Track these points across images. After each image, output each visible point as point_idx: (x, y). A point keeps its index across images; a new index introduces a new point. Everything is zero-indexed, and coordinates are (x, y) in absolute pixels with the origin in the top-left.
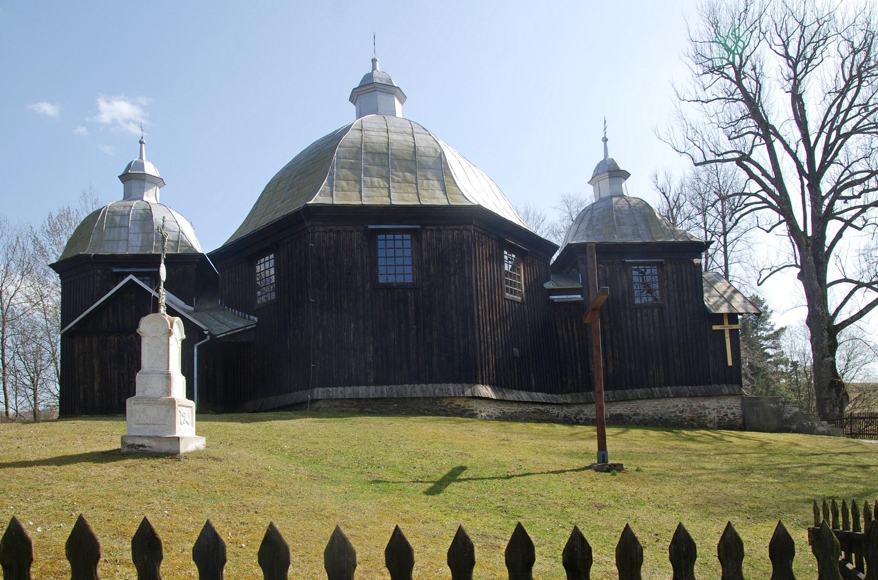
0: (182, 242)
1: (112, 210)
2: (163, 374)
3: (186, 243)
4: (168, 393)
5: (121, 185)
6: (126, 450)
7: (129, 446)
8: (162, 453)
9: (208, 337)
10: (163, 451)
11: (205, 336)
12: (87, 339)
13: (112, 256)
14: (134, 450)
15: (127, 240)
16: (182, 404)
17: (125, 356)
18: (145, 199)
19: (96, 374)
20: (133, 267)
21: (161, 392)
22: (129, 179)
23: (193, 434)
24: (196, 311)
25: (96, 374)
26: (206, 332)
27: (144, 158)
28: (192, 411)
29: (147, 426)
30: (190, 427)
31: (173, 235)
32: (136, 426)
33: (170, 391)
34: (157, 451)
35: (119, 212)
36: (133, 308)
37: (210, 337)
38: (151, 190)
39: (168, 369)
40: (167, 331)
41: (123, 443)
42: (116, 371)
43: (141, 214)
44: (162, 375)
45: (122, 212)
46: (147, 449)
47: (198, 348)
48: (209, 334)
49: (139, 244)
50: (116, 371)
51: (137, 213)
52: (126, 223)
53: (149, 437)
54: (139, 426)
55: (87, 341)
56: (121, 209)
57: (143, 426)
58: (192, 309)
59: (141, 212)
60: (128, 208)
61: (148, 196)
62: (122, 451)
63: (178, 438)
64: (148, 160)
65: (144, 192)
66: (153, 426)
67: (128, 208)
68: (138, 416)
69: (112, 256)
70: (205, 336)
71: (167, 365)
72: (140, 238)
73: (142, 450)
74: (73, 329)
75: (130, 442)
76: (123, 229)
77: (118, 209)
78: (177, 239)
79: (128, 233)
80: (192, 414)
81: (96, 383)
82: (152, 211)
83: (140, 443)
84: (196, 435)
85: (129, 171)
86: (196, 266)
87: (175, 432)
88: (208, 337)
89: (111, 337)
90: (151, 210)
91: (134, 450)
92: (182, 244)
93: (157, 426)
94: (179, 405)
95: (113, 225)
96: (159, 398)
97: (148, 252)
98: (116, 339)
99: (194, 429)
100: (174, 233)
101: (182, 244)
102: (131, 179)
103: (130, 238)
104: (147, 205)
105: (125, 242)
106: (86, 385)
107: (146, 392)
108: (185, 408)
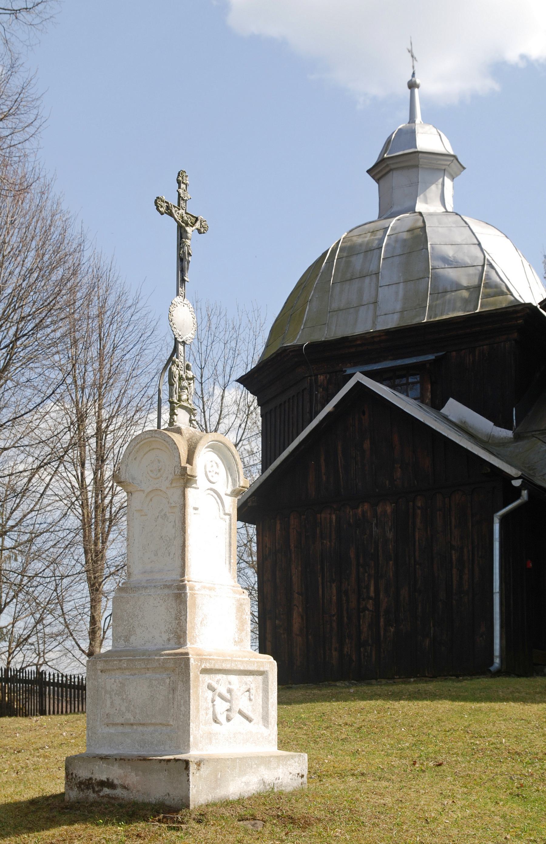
0: (487, 286)
1: (348, 244)
2: (169, 587)
3: (497, 286)
4: (179, 637)
5: (374, 185)
6: (74, 794)
7: (81, 783)
8: (149, 804)
9: (525, 493)
10: (153, 800)
11: (516, 493)
12: (278, 522)
13: (345, 339)
14: (92, 796)
15: (375, 303)
16: (217, 667)
17: (352, 555)
18: (420, 207)
19: (296, 595)
20: (385, 359)
21: (165, 637)
22: (388, 172)
23: (272, 748)
24: (518, 437)
25: (296, 595)
26: (517, 483)
27: (419, 119)
28: (266, 683)
29: (127, 729)
30: (257, 727)
31: (469, 275)
32: (107, 730)
33: (185, 633)
34: (140, 798)
35: (361, 245)
36: (367, 445)
37: (529, 495)
38: (433, 187)
39: (183, 574)
40: (178, 471)
41: (69, 777)
42: (334, 585)
43: (405, 240)
44: (166, 591)
45: (368, 243)
46: (119, 792)
47: (504, 520)
48: (527, 483)
49: (398, 307)
50: (334, 585)
51: (396, 241)
52: (373, 268)
53: (122, 760)
54: (112, 730)
55: (278, 527)
56: (367, 239)
57: (120, 729)
58: (508, 434)
59: (405, 236)
60: (379, 235)
61: (426, 201)
62: (66, 797)
63: (187, 763)
64: (426, 120)
65: (417, 197)
66: (140, 728)
67: (379, 235)
68: (108, 703)
69: (344, 341)
70: (516, 493)
71: (178, 563)
72: (401, 293)
73: (108, 796)
74: (250, 504)
75: (83, 773)
76: (367, 280)
77: (360, 240)
78: (476, 282)
79: (377, 287)
80: (266, 691)
81: (295, 615)
82: (428, 230)
83: (104, 778)
84: (279, 748)
85: (385, 155)
86: (516, 335)
87: (186, 745)
88: (525, 493)
89: (323, 515)
90: (424, 228)
91: (92, 796)
92: (488, 290)
93: (151, 729)
94: (205, 671)
95: (348, 276)
96: (158, 652)
97: (416, 321)
98: (334, 517)
99: (273, 730)
100: (471, 270)
101: (488, 290)
102: (391, 170)
103: (380, 296)
104: (417, 220)
105: (372, 306)
106: (277, 622)
107: (132, 639)
108: (233, 678)
